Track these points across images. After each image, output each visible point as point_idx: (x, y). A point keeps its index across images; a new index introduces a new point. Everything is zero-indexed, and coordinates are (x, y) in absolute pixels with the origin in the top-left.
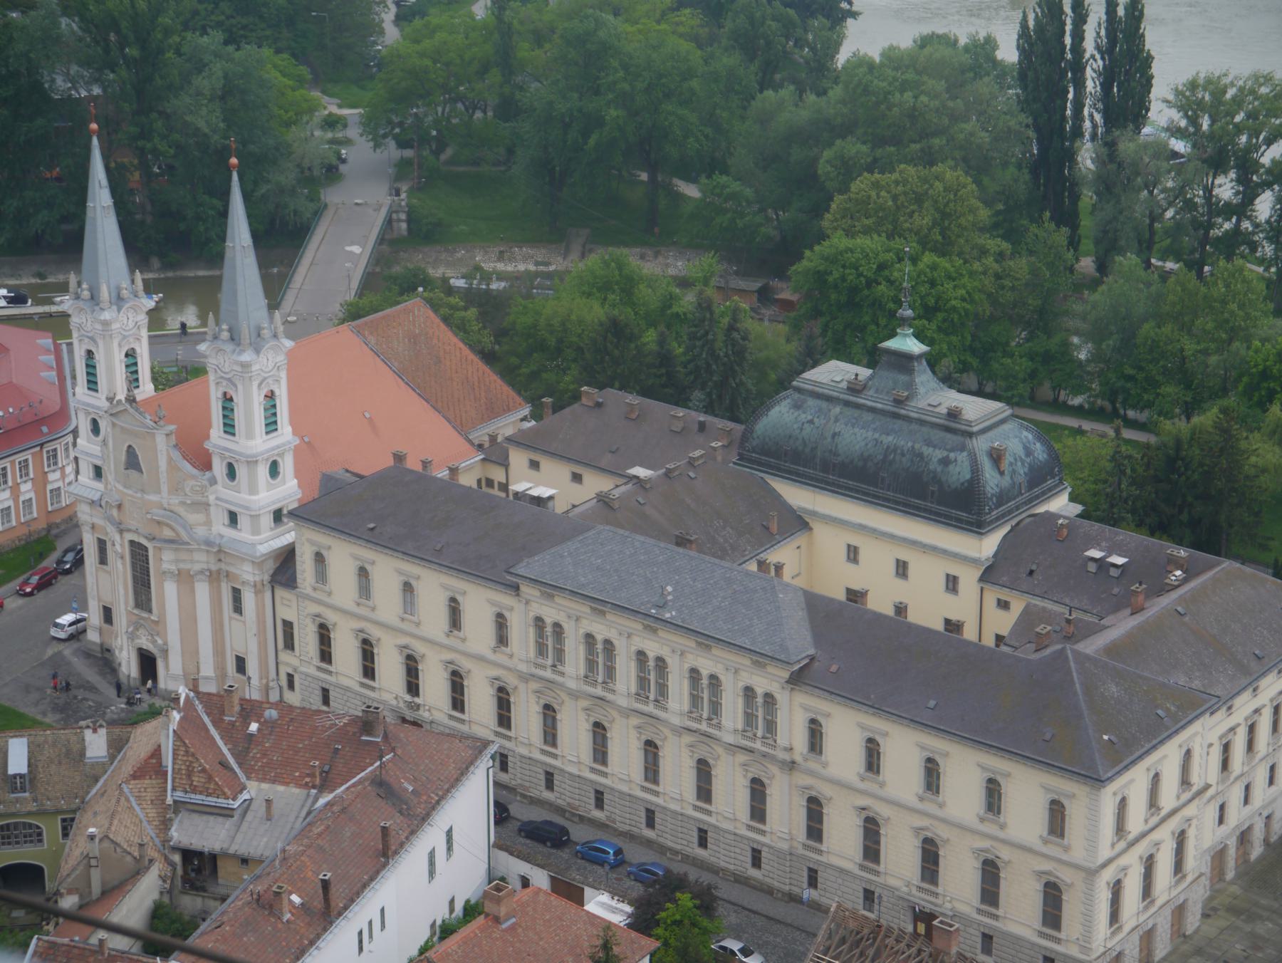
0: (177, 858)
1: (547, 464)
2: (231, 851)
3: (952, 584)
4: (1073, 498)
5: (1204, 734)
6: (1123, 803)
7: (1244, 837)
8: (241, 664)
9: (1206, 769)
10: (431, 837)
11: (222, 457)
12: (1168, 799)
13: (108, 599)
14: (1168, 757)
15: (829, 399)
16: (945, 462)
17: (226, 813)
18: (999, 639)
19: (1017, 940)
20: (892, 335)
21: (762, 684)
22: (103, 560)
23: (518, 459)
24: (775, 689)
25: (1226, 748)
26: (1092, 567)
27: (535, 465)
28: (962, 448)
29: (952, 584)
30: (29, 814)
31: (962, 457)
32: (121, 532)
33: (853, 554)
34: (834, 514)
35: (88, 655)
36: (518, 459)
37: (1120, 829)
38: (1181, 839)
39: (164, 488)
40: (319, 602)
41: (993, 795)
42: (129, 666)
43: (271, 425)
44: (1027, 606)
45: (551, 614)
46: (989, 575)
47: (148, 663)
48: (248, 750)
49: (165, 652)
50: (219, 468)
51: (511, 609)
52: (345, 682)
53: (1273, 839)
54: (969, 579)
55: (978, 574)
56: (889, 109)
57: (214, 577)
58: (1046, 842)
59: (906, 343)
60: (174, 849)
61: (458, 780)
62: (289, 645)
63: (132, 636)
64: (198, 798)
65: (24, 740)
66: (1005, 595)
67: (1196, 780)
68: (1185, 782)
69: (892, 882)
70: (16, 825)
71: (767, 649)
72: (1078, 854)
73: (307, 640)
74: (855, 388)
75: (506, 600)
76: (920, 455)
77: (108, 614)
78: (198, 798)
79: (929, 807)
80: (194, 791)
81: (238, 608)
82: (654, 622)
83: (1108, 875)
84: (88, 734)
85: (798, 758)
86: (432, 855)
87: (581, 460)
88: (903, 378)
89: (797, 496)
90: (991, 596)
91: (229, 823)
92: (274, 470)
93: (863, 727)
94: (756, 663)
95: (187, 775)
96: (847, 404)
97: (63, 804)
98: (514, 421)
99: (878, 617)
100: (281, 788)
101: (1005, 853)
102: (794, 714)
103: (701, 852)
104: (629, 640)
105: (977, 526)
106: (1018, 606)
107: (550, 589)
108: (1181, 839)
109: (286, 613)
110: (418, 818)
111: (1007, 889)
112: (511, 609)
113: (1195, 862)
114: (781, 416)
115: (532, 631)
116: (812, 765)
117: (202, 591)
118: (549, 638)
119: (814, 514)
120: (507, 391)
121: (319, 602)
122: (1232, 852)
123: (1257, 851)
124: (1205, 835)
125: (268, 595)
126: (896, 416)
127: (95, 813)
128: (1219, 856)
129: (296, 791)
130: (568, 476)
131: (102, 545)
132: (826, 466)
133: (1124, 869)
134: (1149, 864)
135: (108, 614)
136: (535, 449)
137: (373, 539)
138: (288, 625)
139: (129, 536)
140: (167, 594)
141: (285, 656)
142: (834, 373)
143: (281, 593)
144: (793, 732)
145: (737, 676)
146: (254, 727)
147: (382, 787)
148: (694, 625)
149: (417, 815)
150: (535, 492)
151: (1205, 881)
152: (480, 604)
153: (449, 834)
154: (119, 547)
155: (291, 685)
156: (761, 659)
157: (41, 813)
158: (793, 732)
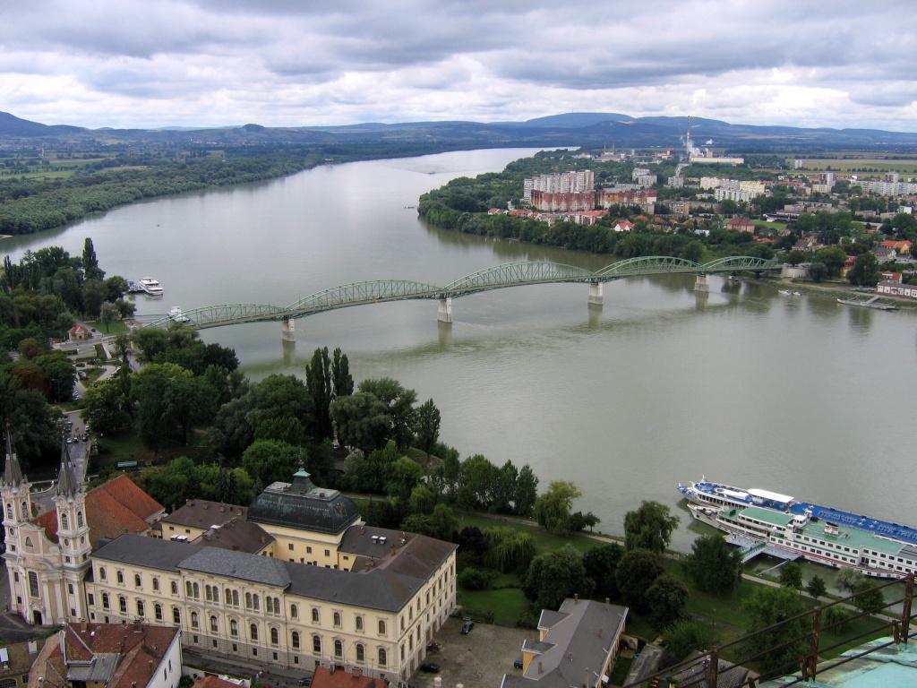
1: (176, 528)
2: (92, 679)
3: (327, 553)
4: (362, 520)
5: (422, 593)
6: (403, 619)
7: (434, 624)
8: (74, 613)
10: (164, 665)
11: (63, 537)
13: (19, 594)
14: (413, 602)
15: (277, 495)
17: (87, 666)
19: (305, 656)
20: (298, 471)
22: (17, 579)
23: (165, 527)
24: (278, 596)
26: (375, 542)
27: (172, 528)
29: (327, 553)
30: (11, 676)
32: (25, 569)
33: (291, 547)
34: (330, 541)
35: (13, 615)
36: (165, 527)
37: (402, 627)
38: (419, 628)
40: (103, 586)
41: (337, 618)
42: (29, 617)
43: (80, 524)
44: (357, 558)
45: (192, 580)
46: (340, 548)
47: (38, 616)
49: (45, 611)
50: (61, 541)
51: (178, 580)
52: (114, 613)
54: (333, 551)
55: (336, 548)
57: (62, 581)
58: (379, 636)
59: (302, 473)
60: (70, 681)
61: (170, 643)
62: (92, 603)
63: (31, 607)
64: (76, 662)
65: (5, 649)
66: (346, 555)
69: (325, 657)
70: (6, 680)
71: (274, 583)
73: (99, 600)
74: (286, 490)
75: (175, 577)
77: (19, 600)
78: (76, 662)
79: (382, 638)
80: (75, 659)
81: (71, 592)
82: (232, 577)
84: (30, 643)
87: (189, 525)
88: (303, 485)
89: (269, 529)
90: (342, 555)
91: (90, 669)
92: (82, 539)
93: (134, 572)
94: (230, 581)
95: (70, 655)
96: (284, 495)
97: (23, 670)
98: (161, 514)
99: (298, 564)
101: (321, 633)
102: (286, 602)
103: (255, 657)
104: (221, 584)
105: (334, 532)
107: (192, 571)
108: (419, 628)
109: (90, 591)
110: (160, 659)
111: (323, 645)
112: (178, 580)
113: (423, 635)
114: (262, 502)
116: (294, 621)
117: (58, 587)
118: (192, 589)
119: (275, 535)
120: (157, 504)
121: (103, 586)
123: (438, 628)
124: (425, 626)
127: (38, 672)
129: (112, 654)
130: (184, 531)
131: (16, 575)
133: (405, 641)
134: (411, 638)
135: (19, 600)
136: (172, 523)
137: (123, 560)
138: (91, 596)
139: (28, 570)
140: (44, 590)
142: (278, 486)
143: (88, 584)
145: (262, 592)
146: (93, 633)
147: (146, 650)
148: (247, 577)
149: (159, 657)
150: (180, 538)
152: (165, 579)
154: (23, 574)
155: (93, 617)
156: (272, 586)
157: (14, 675)
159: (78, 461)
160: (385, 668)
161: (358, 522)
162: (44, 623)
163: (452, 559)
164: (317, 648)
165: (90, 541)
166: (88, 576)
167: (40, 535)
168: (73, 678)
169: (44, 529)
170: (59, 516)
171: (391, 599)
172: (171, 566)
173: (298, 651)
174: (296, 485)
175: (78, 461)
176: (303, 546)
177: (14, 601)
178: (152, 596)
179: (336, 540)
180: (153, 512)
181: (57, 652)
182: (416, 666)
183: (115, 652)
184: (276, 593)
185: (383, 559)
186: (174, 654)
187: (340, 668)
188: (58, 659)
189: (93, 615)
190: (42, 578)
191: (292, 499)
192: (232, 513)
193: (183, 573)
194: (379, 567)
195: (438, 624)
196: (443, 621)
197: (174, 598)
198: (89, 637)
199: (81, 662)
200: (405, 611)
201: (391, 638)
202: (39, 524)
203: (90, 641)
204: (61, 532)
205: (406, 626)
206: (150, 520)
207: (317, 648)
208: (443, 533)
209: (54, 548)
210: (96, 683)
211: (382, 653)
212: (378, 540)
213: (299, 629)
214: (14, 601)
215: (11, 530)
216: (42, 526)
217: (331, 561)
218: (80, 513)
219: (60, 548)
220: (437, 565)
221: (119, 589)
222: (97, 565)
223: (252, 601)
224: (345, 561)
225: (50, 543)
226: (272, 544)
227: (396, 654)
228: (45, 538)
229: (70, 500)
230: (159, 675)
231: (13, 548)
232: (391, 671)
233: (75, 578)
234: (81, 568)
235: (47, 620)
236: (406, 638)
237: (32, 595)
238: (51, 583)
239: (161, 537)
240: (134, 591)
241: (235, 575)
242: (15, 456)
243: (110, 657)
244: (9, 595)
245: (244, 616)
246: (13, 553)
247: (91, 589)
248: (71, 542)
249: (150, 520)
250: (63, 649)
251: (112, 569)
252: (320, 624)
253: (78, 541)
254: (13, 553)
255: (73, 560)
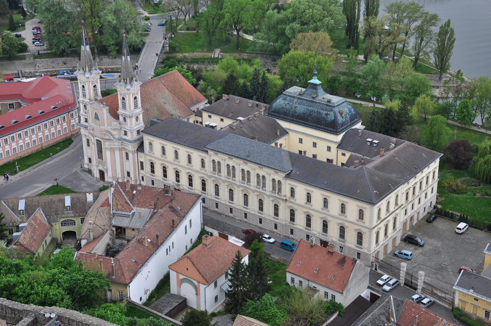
0: (114, 229)
1: (213, 116)
3: (329, 149)
4: (362, 124)
5: (402, 190)
7: (412, 219)
8: (129, 174)
9: (402, 200)
10: (186, 222)
11: (122, 116)
12: (392, 209)
15: (293, 97)
16: (327, 114)
17: (127, 216)
18: (343, 164)
21: (277, 178)
23: (205, 115)
25: (407, 194)
26: (369, 144)
27: (210, 117)
28: (332, 110)
29: (329, 149)
31: (332, 113)
36: (205, 115)
37: (379, 217)
39: (106, 125)
40: (151, 156)
42: (97, 174)
43: (136, 106)
44: (351, 154)
45: (217, 159)
47: (102, 174)
48: (133, 198)
49: (107, 170)
50: (121, 118)
53: (420, 219)
54: (334, 147)
56: (306, 15)
57: (120, 150)
58: (358, 221)
60: (114, 226)
62: (142, 168)
66: (344, 152)
67: (399, 203)
68: (396, 204)
71: (279, 168)
72: (367, 224)
73: (147, 167)
75: (204, 155)
76: (320, 113)
77: (90, 160)
81: (127, 158)
82: (246, 160)
83: (375, 230)
85: (288, 199)
86: (186, 227)
87: (224, 115)
88: (314, 91)
89: (284, 124)
90: (340, 152)
92: (137, 119)
94: (275, 172)
96: (299, 98)
100: (143, 209)
102: (287, 185)
104: (239, 165)
106: (348, 154)
107: (217, 151)
109: (141, 159)
113: (399, 226)
114: (280, 102)
115: (212, 164)
116: (292, 200)
117: (117, 153)
118: (217, 166)
119: (290, 130)
122: (408, 222)
123: (415, 222)
125: (136, 154)
126: (313, 102)
128: (405, 224)
131: (88, 140)
132: (293, 116)
135: (90, 160)
138: (142, 163)
139: (96, 138)
140: (107, 154)
141: (141, 171)
142: (295, 90)
143: (139, 154)
144: (286, 191)
146: (135, 192)
150: (211, 125)
151: (401, 231)
152: (197, 156)
153: (190, 221)
154: (93, 141)
155: (143, 180)
156: (277, 170)
158: (286, 191)
159: (149, 59)
160: (361, 248)
161: (359, 126)
162: (106, 180)
163: (435, 165)
164: (309, 224)
165: (143, 120)
166: (141, 148)
167: (104, 112)
168: (116, 224)
169: (108, 108)
170: (120, 98)
171: (373, 191)
172: (202, 147)
173: (310, 230)
174: (310, 91)
175: (149, 59)
176: (325, 145)
177: (86, 161)
178: (186, 168)
179: (339, 138)
180: (198, 102)
181: (106, 203)
182: (389, 250)
183: (150, 208)
184: (280, 177)
185: (373, 159)
186: (195, 215)
187: (324, 244)
188: (106, 208)
189: (143, 178)
190: (106, 145)
191: (305, 102)
192: (256, 109)
193: (210, 152)
194: (366, 166)
195: (416, 217)
196: (421, 216)
197: (176, 162)
198: (130, 193)
199: (123, 213)
200: (383, 204)
201: (367, 224)
202: (104, 103)
203: (132, 198)
204: (120, 111)
205: (383, 216)
206: (194, 108)
207: (309, 224)
208: (432, 144)
209: (115, 123)
210: (133, 230)
211: (360, 236)
212: (371, 143)
213: (295, 207)
214: (86, 161)
215: (85, 106)
216: (107, 106)
217: (332, 155)
218: (135, 98)
219: (120, 123)
220: (419, 169)
221: (323, 213)
222: (147, 139)
223: (231, 171)
224: (343, 157)
225: (112, 119)
226: (286, 137)
227: (370, 237)
228: (109, 115)
229: (128, 87)
230: (180, 229)
231: (86, 121)
232: (365, 251)
233: (131, 148)
234: (135, 141)
235: (108, 178)
236: (382, 226)
237: (99, 158)
238: (112, 150)
239: (201, 123)
240: (174, 161)
241: (249, 159)
242: (88, 48)
243: (146, 212)
244: (83, 157)
245: (224, 182)
246: (86, 124)
247: (142, 157)
248: (128, 120)
249: (194, 108)
250: (111, 202)
251: (158, 143)
252: (179, 162)
253: (134, 119)
254: (86, 124)
255: (129, 133)
